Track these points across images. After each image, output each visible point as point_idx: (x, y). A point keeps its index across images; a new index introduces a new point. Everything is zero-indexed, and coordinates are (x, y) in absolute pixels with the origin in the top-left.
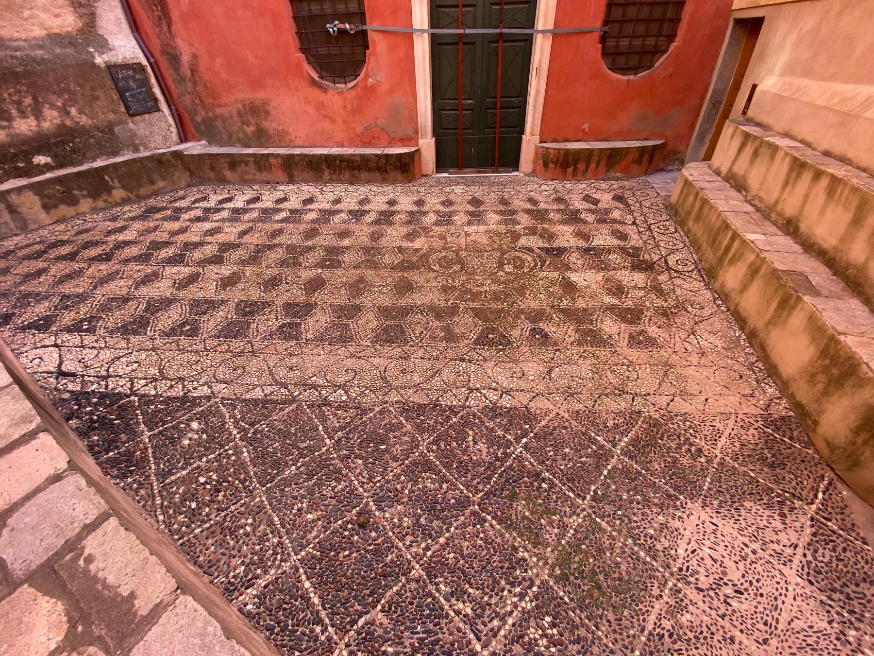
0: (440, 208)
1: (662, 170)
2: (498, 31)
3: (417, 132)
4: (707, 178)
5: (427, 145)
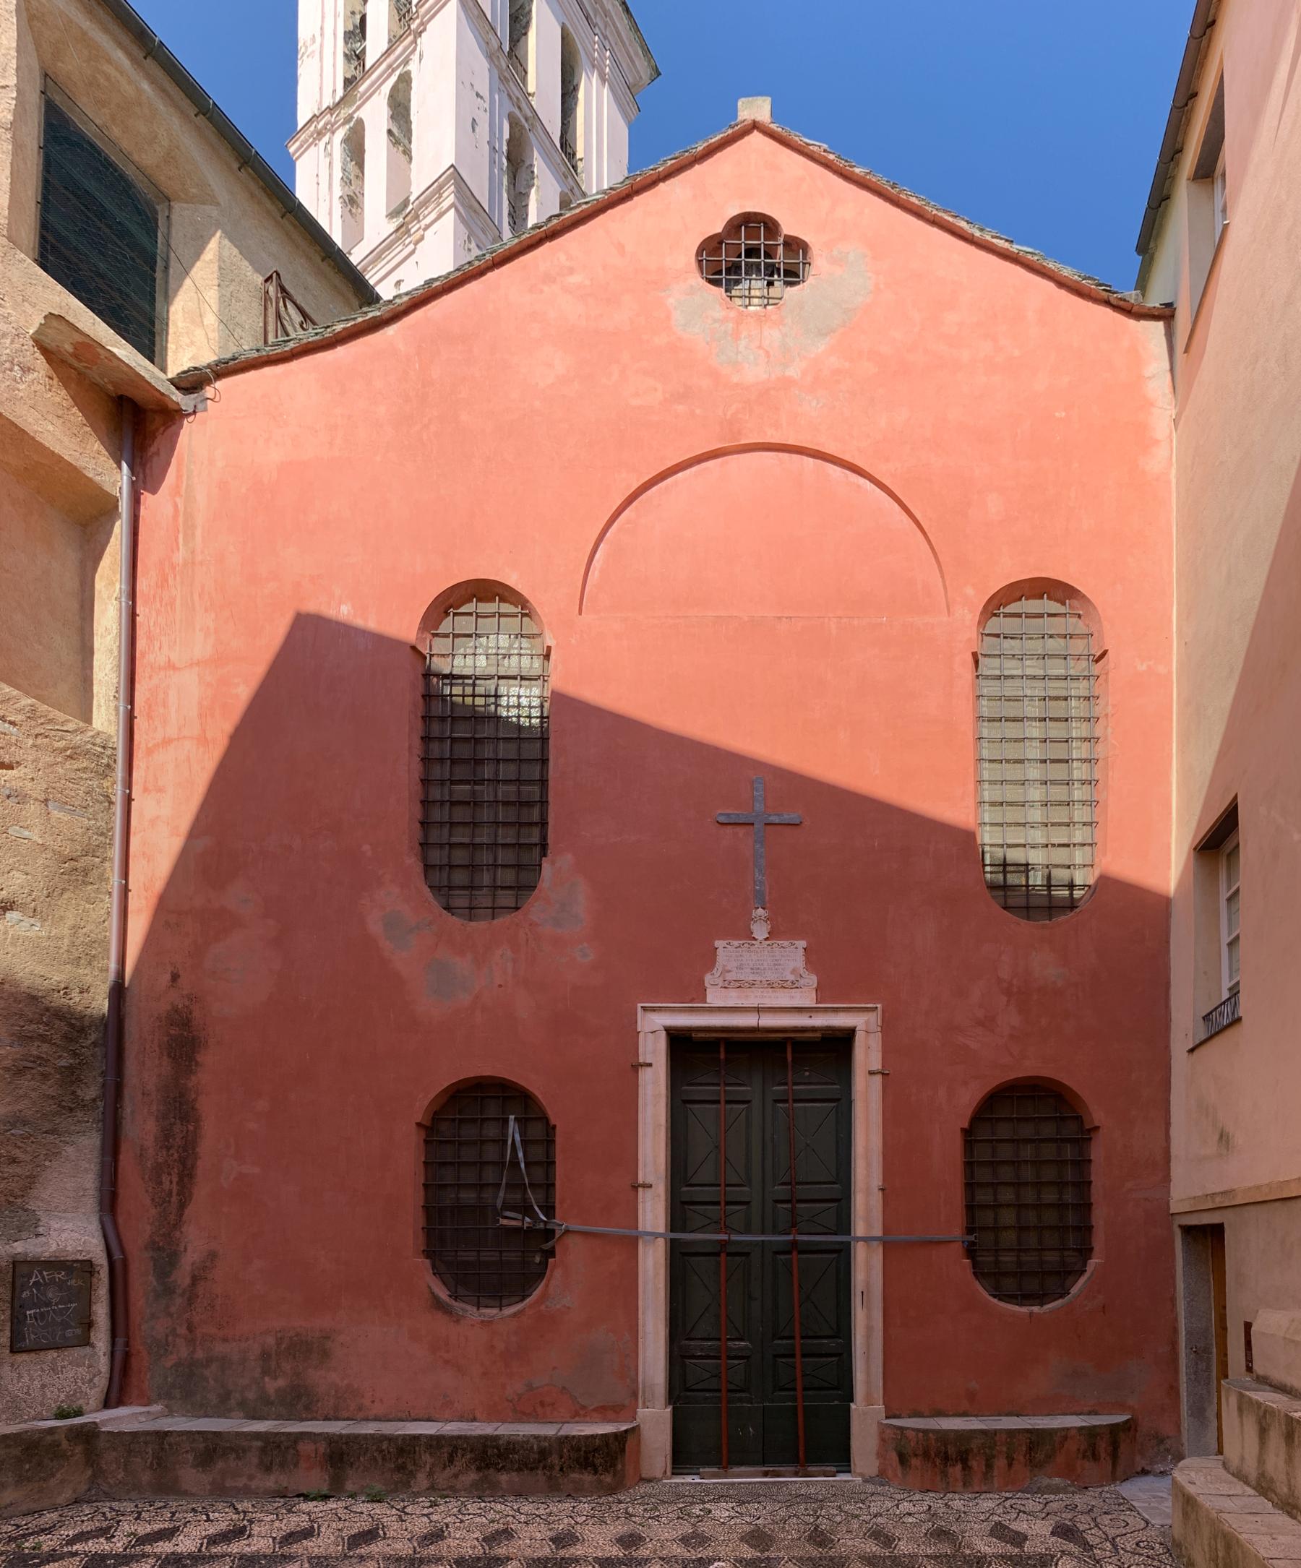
0: (678, 1550)
1: (1144, 1472)
2: (790, 1237)
3: (635, 1394)
4: (1224, 1489)
5: (655, 1421)
